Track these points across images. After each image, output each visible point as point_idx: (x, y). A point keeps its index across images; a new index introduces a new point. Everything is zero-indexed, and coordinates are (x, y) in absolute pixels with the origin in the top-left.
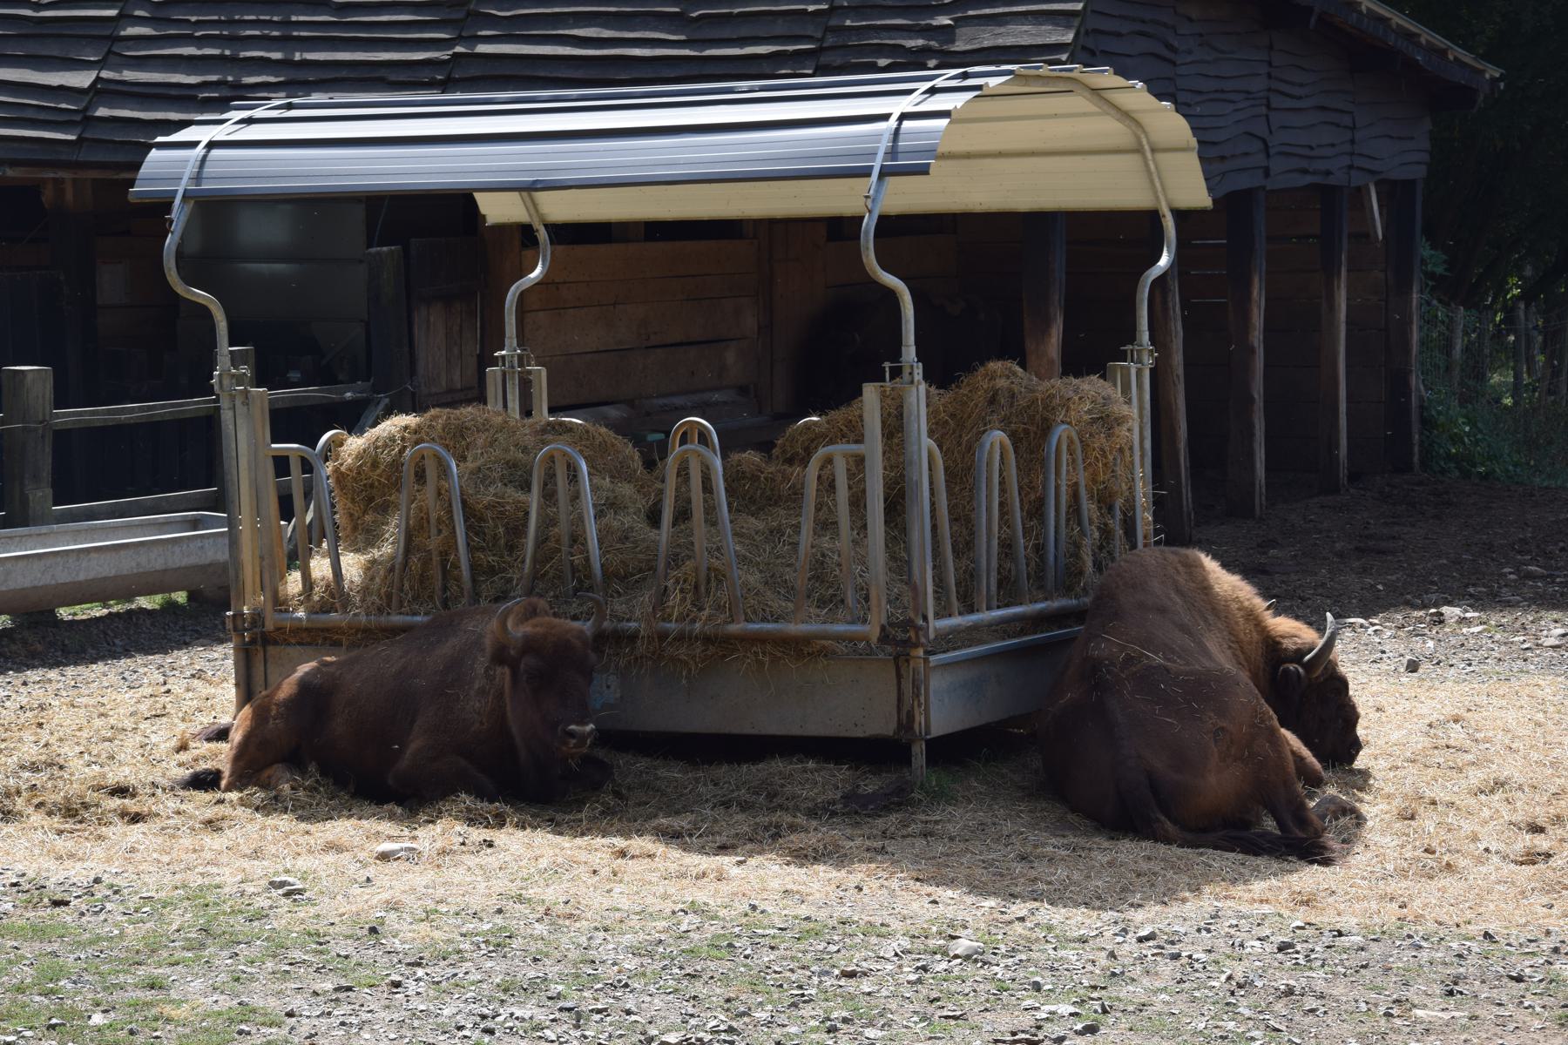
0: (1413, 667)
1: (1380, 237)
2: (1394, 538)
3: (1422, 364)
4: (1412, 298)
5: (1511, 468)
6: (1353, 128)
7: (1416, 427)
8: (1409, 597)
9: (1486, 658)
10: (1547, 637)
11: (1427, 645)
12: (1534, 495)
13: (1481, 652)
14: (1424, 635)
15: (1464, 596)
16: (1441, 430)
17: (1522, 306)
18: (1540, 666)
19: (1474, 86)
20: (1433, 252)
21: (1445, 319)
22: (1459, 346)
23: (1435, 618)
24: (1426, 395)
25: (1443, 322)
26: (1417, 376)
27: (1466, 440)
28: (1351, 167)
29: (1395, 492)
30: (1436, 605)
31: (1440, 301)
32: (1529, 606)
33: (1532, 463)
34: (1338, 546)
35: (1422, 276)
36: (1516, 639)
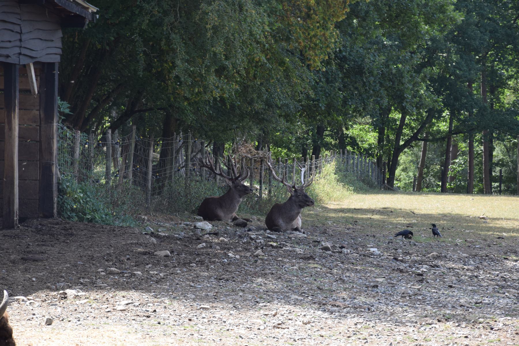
0: (49, 322)
1: (37, 92)
2: (43, 253)
3: (59, 160)
4: (53, 126)
5: (104, 216)
6: (21, 33)
7: (55, 194)
8: (49, 284)
9: (88, 317)
10: (119, 305)
11: (58, 310)
12: (115, 231)
13: (85, 313)
14: (56, 305)
15: (78, 284)
16: (68, 195)
17: (110, 131)
18: (114, 321)
19: (84, 15)
20: (62, 102)
21: (70, 137)
22: (78, 151)
23: (62, 296)
24: (61, 177)
25: (70, 139)
26: (56, 167)
27: (81, 201)
28: (20, 54)
29: (44, 228)
30: (63, 289)
31: (68, 127)
32: (111, 289)
33: (115, 214)
34: (13, 257)
35: (58, 114)
36: (103, 306)
